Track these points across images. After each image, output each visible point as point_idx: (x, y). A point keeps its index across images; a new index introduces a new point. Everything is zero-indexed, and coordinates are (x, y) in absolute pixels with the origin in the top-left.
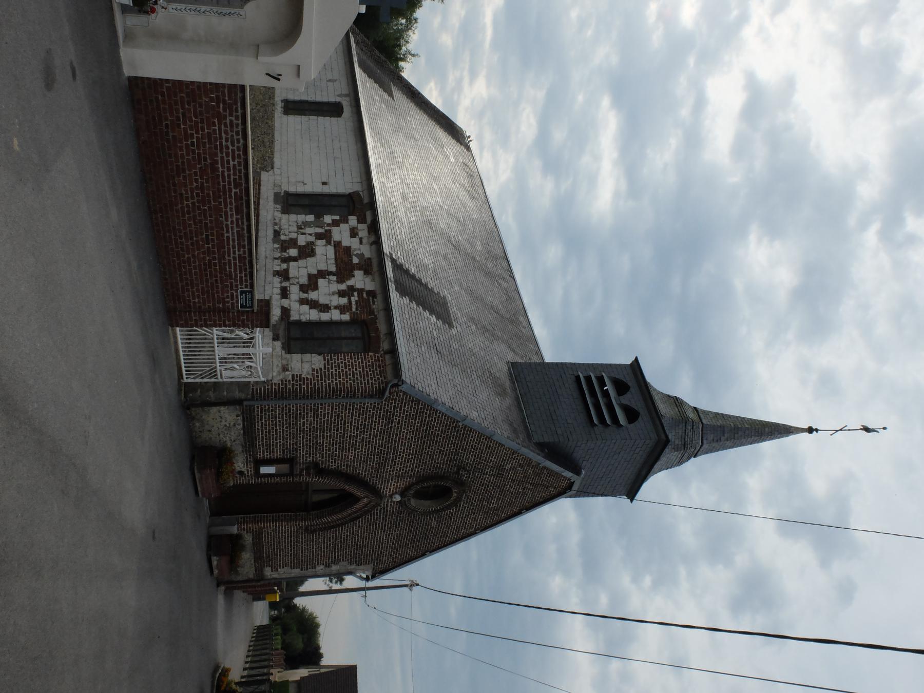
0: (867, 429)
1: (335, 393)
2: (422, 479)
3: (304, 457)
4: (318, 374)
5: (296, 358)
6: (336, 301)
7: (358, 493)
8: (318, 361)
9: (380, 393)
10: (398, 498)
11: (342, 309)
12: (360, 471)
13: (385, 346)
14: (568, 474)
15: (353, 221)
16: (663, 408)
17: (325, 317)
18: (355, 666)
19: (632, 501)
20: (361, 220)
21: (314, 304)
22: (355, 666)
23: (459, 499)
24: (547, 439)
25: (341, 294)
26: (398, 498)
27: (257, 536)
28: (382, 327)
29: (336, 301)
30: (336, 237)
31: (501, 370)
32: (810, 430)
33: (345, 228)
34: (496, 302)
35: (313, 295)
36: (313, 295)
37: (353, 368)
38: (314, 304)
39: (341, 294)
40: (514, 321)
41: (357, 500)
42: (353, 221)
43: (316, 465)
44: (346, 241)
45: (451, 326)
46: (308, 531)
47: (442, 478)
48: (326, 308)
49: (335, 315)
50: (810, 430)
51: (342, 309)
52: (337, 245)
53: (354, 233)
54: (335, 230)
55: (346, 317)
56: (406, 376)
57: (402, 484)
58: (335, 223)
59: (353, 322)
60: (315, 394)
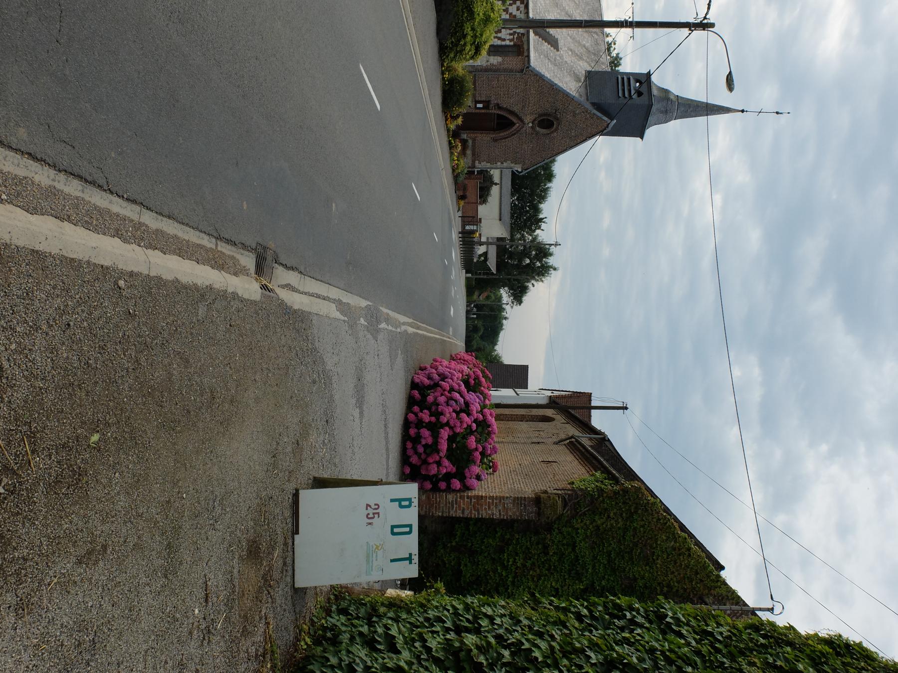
0: (777, 113)
1: (505, 70)
2: (540, 115)
3: (494, 101)
4: (500, 64)
5: (492, 57)
6: (508, 37)
7: (514, 120)
8: (499, 59)
9: (522, 71)
10: (531, 125)
11: (510, 40)
12: (516, 109)
13: (526, 54)
14: (605, 118)
15: (518, 3)
16: (655, 92)
17: (503, 43)
18: (527, 367)
19: (642, 138)
20: (522, 3)
21: (499, 38)
22: (527, 367)
23: (557, 129)
24: (596, 101)
25: (511, 34)
26: (531, 125)
27: (474, 140)
28: (525, 47)
29: (508, 37)
30: (510, 11)
31: (582, 75)
32: (743, 111)
33: (514, 6)
34: (587, 45)
35: (499, 35)
36: (499, 35)
37: (513, 62)
38: (499, 38)
39: (511, 34)
40: (698, 106)
41: (513, 124)
42: (518, 3)
43: (498, 105)
44: (515, 12)
45: (558, 50)
46: (495, 140)
47: (549, 115)
48: (504, 40)
49: (508, 43)
50: (743, 111)
51: (510, 40)
52: (511, 14)
53: (518, 9)
54: (510, 8)
55: (512, 43)
56: (532, 64)
57: (533, 117)
58: (511, 5)
59: (515, 45)
60: (497, 70)
